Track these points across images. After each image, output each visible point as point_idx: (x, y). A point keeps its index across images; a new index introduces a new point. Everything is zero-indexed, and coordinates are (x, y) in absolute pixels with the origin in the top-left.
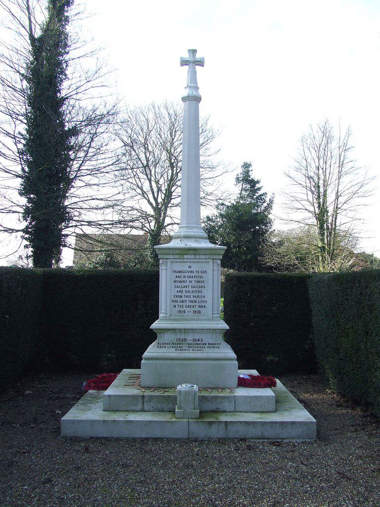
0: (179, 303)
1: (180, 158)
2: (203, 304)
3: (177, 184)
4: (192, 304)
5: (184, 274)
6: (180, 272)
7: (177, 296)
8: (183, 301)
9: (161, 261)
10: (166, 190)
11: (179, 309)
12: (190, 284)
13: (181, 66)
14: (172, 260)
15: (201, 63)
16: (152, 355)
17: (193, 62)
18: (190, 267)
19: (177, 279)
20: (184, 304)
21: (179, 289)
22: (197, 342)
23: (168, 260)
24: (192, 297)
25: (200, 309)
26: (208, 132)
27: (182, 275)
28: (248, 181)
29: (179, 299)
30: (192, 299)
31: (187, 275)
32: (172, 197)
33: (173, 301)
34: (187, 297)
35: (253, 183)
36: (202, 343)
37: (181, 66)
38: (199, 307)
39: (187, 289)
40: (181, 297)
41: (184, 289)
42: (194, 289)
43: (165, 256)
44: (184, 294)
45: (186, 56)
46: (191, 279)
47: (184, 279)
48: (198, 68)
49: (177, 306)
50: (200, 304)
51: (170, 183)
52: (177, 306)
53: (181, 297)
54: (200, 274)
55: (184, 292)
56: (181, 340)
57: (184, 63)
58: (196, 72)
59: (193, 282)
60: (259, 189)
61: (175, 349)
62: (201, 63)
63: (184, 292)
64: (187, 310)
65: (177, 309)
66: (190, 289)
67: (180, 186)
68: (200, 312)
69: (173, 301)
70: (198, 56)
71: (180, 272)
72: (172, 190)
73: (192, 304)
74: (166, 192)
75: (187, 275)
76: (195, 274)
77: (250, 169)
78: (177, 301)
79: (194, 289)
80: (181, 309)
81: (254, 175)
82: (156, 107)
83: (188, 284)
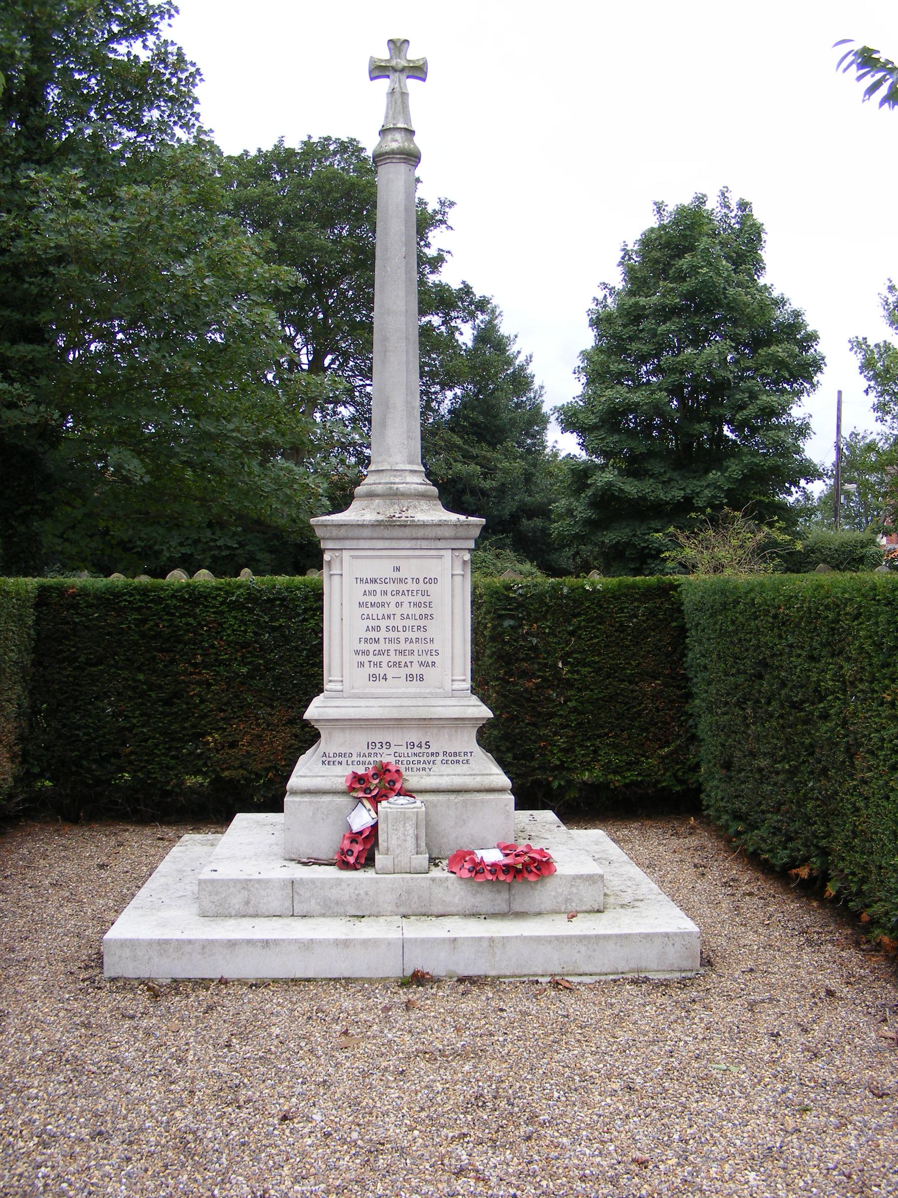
2: (430, 659)
4: (403, 659)
5: (384, 587)
7: (366, 640)
12: (399, 611)
18: (398, 569)
19: (371, 599)
20: (384, 659)
21: (371, 623)
24: (402, 640)
25: (423, 670)
27: (378, 587)
29: (372, 647)
31: (390, 587)
34: (390, 640)
38: (421, 664)
39: (390, 623)
40: (377, 641)
41: (383, 624)
42: (407, 623)
50: (423, 658)
53: (377, 641)
54: (422, 586)
55: (383, 629)
59: (406, 605)
73: (403, 659)
78: (366, 653)
79: (407, 623)
83: (392, 609)
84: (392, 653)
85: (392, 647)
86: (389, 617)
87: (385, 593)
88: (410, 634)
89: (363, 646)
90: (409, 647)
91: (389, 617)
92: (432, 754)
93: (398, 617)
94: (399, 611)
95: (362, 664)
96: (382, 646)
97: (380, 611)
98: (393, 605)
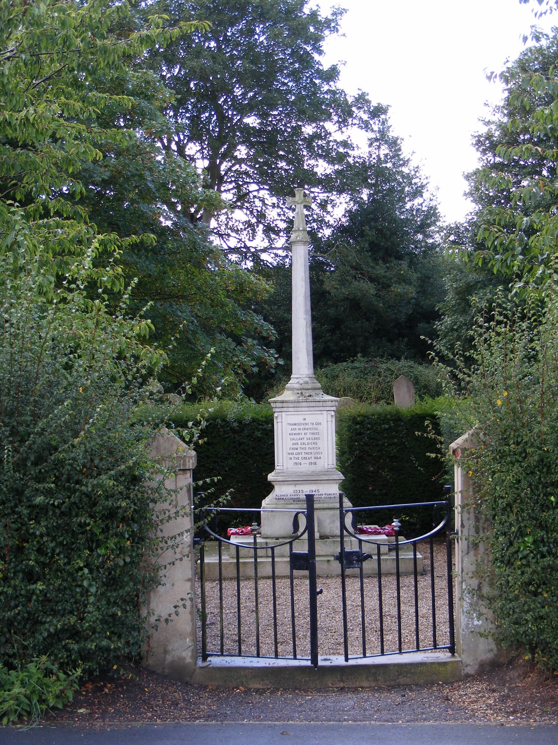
2: (319, 456)
5: (299, 427)
12: (305, 437)
20: (300, 456)
21: (294, 442)
27: (297, 427)
29: (295, 451)
30: (307, 451)
31: (302, 427)
33: (289, 454)
38: (315, 458)
39: (302, 441)
40: (297, 449)
41: (299, 442)
47: (300, 432)
50: (316, 456)
54: (315, 426)
64: (303, 462)
66: (305, 441)
78: (292, 454)
79: (309, 441)
80: (297, 461)
83: (303, 436)
85: (303, 451)
88: (310, 446)
89: (291, 451)
90: (310, 451)
94: (305, 437)
96: (299, 451)
97: (298, 437)
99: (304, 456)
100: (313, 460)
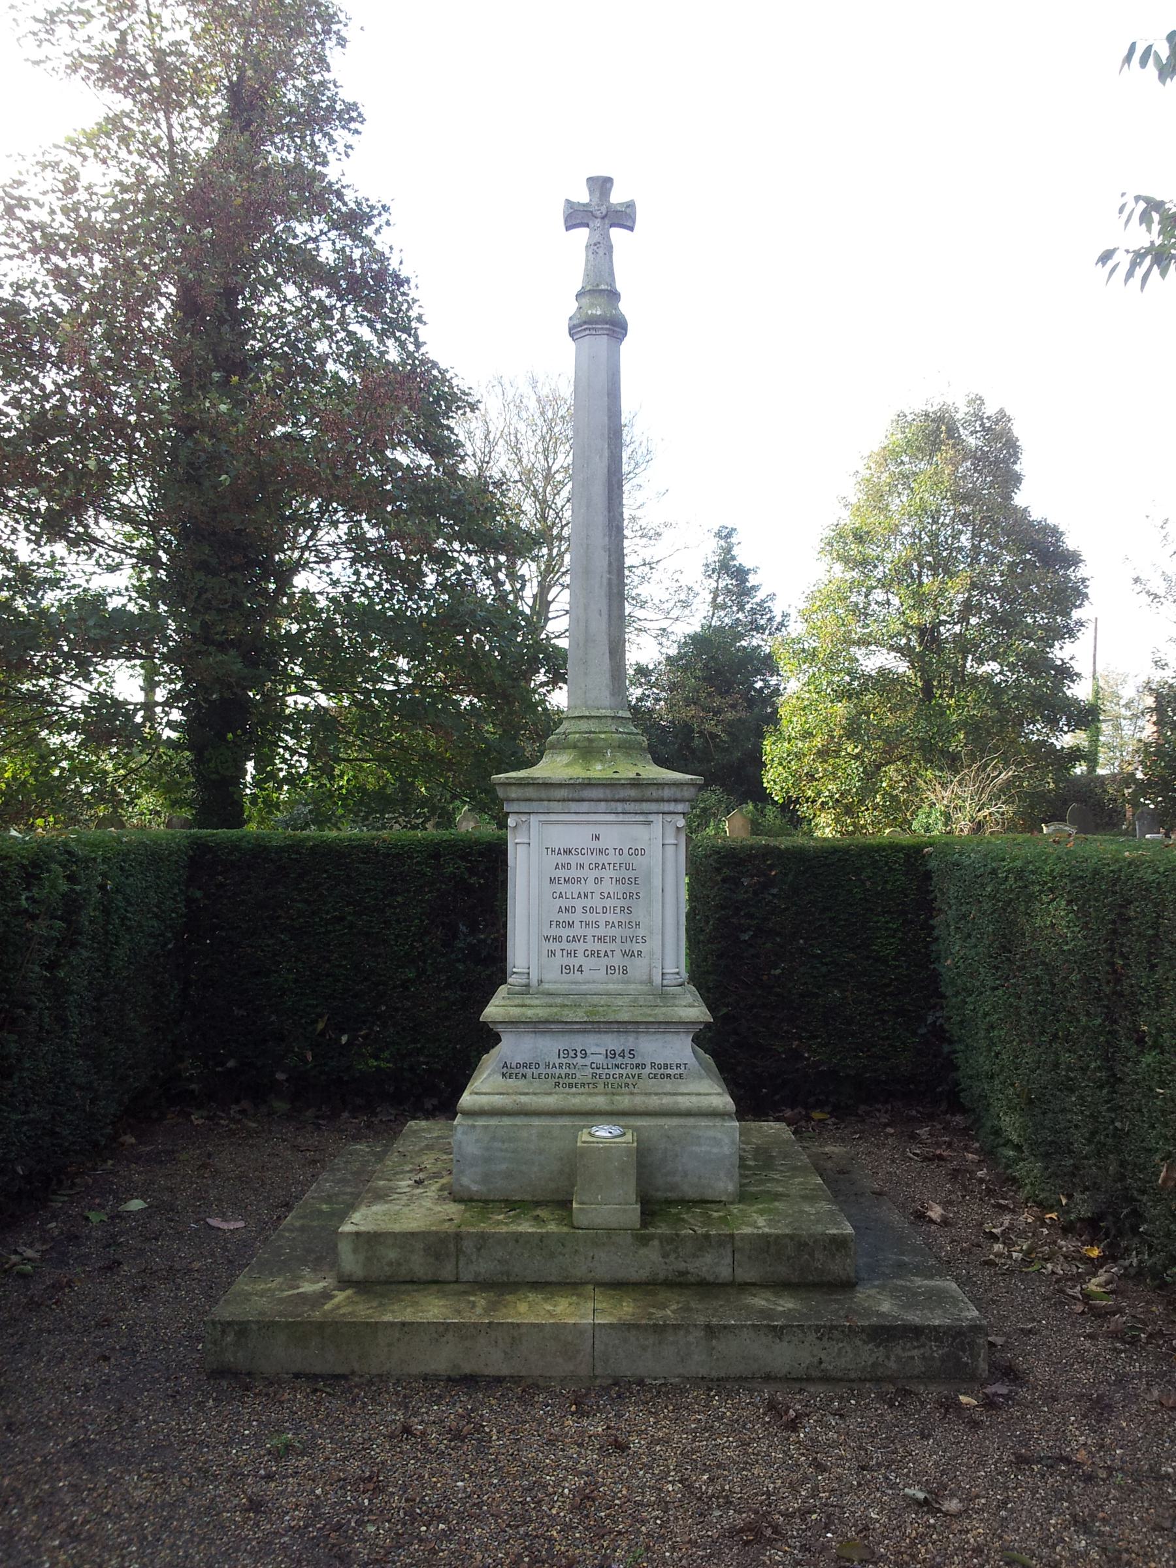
0: (565, 945)
1: (567, 514)
2: (636, 947)
3: (561, 581)
4: (603, 947)
5: (581, 859)
6: (568, 852)
8: (575, 939)
9: (511, 821)
10: (535, 596)
11: (567, 961)
12: (597, 889)
13: (568, 229)
14: (543, 817)
15: (624, 217)
16: (484, 1101)
17: (600, 214)
18: (597, 838)
19: (562, 873)
20: (580, 947)
21: (563, 903)
22: (619, 1060)
23: (533, 819)
25: (627, 961)
26: (637, 444)
27: (572, 859)
28: (733, 576)
29: (565, 932)
30: (601, 931)
31: (586, 860)
32: (550, 615)
33: (547, 938)
34: (587, 924)
35: (741, 574)
36: (635, 1061)
37: (568, 229)
39: (588, 903)
40: (571, 925)
41: (579, 904)
43: (524, 807)
44: (576, 917)
45: (582, 196)
46: (597, 873)
48: (616, 234)
49: (559, 953)
50: (627, 947)
51: (544, 579)
52: (559, 953)
53: (571, 925)
54: (626, 858)
55: (579, 910)
56: (572, 1054)
57: (575, 217)
58: (611, 247)
59: (607, 881)
60: (754, 588)
61: (552, 1081)
62: (624, 217)
63: (579, 910)
64: (588, 963)
65: (560, 960)
66: (596, 901)
67: (568, 587)
68: (625, 970)
69: (547, 938)
70: (617, 197)
71: (568, 852)
72: (550, 598)
73: (603, 947)
74: (535, 601)
75: (586, 860)
76: (612, 858)
77: (734, 540)
79: (608, 903)
80: (572, 961)
81: (743, 557)
82: (505, 381)
83: (590, 886)
84: (589, 939)
85: (590, 932)
86: (586, 896)
87: (582, 866)
88: (610, 917)
91: (586, 896)
92: (637, 1066)
93: (597, 896)
94: (597, 889)
95: (553, 953)
96: (577, 931)
97: (576, 888)
98: (591, 881)
99: (592, 945)
100: (617, 960)
